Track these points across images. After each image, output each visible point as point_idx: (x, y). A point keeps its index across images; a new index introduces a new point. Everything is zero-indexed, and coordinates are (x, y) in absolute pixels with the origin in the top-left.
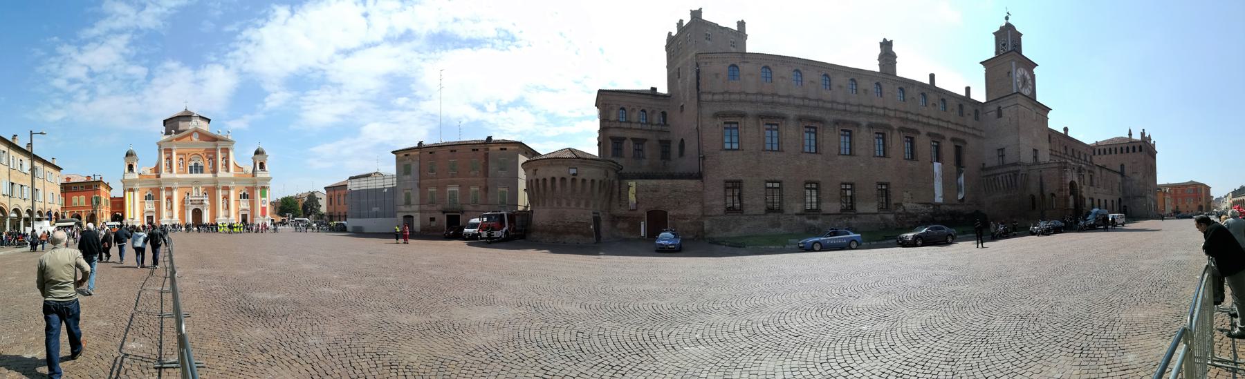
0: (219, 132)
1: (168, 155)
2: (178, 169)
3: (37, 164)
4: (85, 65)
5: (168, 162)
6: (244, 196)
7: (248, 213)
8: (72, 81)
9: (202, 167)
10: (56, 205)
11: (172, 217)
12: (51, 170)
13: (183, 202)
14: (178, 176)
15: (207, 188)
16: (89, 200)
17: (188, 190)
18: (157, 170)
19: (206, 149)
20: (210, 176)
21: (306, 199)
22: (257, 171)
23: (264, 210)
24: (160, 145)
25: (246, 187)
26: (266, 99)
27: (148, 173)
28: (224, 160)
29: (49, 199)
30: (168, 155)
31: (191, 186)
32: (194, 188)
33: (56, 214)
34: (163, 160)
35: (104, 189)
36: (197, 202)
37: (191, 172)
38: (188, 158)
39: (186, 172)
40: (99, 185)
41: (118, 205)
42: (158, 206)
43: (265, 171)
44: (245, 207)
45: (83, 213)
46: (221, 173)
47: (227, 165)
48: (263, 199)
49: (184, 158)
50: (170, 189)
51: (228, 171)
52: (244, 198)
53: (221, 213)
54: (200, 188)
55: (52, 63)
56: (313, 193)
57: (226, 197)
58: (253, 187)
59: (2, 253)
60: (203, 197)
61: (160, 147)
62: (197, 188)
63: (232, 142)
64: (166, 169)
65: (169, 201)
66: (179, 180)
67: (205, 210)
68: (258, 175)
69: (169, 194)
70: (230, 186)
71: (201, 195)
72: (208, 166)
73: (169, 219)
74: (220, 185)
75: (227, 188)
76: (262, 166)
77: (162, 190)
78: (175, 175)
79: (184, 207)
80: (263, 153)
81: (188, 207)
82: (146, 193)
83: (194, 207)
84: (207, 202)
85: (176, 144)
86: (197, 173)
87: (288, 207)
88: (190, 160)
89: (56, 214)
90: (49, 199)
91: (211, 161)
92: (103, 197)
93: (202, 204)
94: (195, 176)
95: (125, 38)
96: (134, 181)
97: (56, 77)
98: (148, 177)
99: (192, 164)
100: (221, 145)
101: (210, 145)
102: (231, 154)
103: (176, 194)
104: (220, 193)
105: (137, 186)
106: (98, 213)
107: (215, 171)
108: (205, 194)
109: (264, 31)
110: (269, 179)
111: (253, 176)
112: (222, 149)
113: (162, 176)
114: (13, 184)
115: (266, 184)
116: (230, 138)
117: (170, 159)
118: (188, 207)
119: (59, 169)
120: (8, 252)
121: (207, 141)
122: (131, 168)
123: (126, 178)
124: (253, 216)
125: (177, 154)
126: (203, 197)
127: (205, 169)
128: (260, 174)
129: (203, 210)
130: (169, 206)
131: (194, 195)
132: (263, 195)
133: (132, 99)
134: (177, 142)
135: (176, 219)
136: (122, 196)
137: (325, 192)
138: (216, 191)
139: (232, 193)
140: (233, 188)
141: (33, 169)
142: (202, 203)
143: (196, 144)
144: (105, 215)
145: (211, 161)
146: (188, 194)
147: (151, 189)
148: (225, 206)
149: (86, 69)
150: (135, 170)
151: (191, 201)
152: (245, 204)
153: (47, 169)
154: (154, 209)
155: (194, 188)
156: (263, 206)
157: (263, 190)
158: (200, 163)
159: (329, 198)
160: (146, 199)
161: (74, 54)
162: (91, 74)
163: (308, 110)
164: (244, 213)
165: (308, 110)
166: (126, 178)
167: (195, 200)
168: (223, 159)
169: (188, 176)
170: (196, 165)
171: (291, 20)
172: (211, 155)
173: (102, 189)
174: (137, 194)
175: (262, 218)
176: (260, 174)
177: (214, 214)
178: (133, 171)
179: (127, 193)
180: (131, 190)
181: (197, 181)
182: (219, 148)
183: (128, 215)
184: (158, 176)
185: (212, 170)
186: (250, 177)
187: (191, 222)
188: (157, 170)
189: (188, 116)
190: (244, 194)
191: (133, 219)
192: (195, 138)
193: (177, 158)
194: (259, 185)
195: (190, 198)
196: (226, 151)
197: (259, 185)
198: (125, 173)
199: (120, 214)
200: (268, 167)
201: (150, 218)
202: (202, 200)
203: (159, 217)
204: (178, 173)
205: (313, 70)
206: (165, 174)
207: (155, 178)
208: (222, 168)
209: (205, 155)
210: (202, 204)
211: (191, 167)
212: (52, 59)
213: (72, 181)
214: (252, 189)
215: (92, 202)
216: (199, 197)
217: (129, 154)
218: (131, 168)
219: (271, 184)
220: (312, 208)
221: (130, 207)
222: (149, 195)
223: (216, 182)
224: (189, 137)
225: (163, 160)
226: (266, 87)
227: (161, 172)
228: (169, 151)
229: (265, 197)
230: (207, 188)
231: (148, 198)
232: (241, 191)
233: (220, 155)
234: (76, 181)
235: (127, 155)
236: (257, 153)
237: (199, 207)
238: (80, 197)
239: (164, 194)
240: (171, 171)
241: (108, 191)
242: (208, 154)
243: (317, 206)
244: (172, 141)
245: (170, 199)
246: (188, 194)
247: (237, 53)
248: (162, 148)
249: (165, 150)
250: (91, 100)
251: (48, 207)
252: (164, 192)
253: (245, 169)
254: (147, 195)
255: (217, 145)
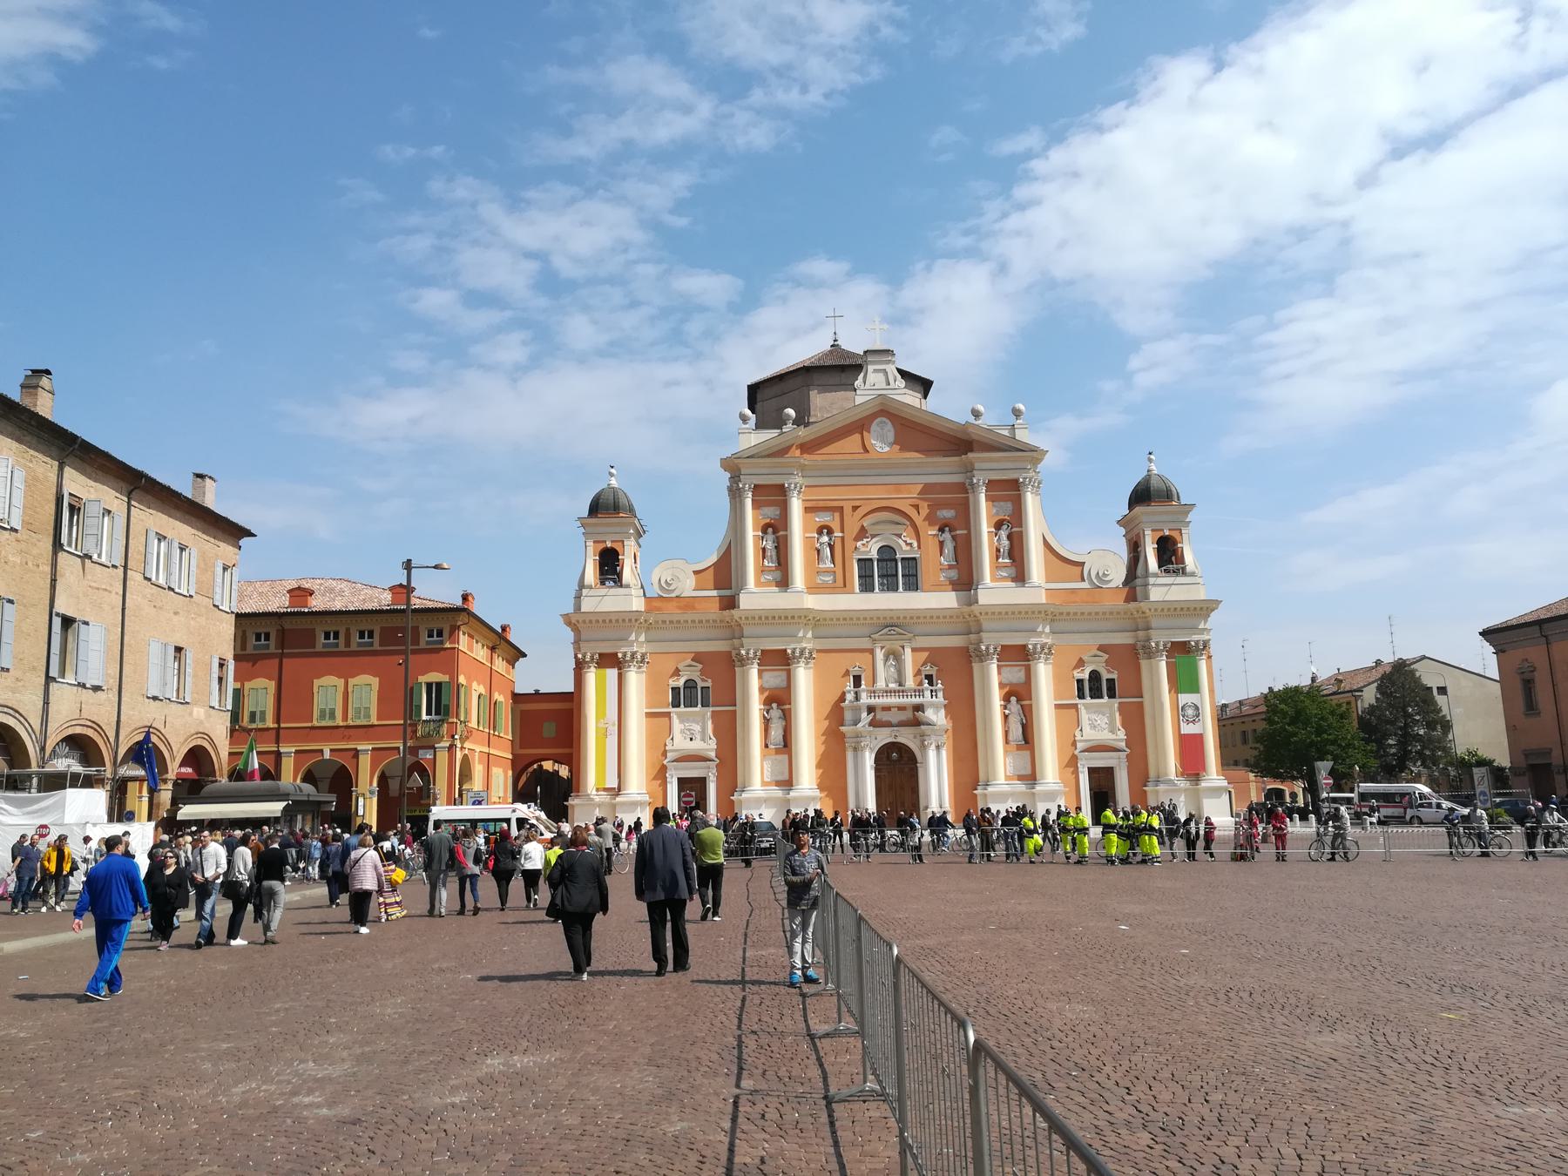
0: (976, 414)
1: (771, 512)
2: (812, 571)
3: (77, 483)
4: (530, 255)
5: (769, 545)
6: (1094, 687)
7: (1120, 766)
8: (477, 299)
9: (911, 562)
10: (199, 712)
11: (788, 783)
12: (180, 530)
13: (835, 718)
14: (812, 602)
15: (935, 656)
16: (401, 699)
17: (858, 663)
18: (725, 574)
19: (927, 489)
20: (948, 600)
21: (1370, 696)
22: (1147, 574)
23: (1191, 748)
24: (733, 467)
25: (1102, 648)
26: (1135, 362)
27: (687, 586)
28: (1003, 533)
29: (154, 671)
30: (771, 512)
31: (865, 643)
32: (880, 655)
33: (197, 757)
34: (751, 533)
35: (481, 653)
36: (894, 717)
37: (867, 587)
38: (852, 527)
39: (845, 587)
40: (454, 629)
41: (549, 730)
42: (729, 733)
43: (1184, 572)
44: (1104, 736)
45: (365, 762)
46: (994, 591)
47: (1016, 555)
48: (1184, 698)
49: (835, 525)
50: (780, 660)
51: (1020, 577)
52: (1096, 693)
53: (1001, 764)
54: (908, 656)
55: (410, 232)
56: (1401, 667)
57: (1019, 695)
58: (1133, 647)
59: (11, 947)
60: (920, 692)
61: (735, 477)
62: (894, 656)
63: (1032, 454)
64: (762, 570)
65: (776, 713)
66: (815, 621)
67: (932, 754)
68: (1156, 594)
69: (775, 679)
70: (1032, 642)
71: (910, 683)
72: (936, 560)
73: (777, 793)
74: (990, 641)
75: (1020, 655)
76: (1169, 552)
77: (744, 662)
78: (802, 597)
79: (843, 735)
80: (1167, 495)
81: (858, 736)
82: (677, 673)
83: (884, 737)
84: (937, 716)
85: (802, 468)
86: (892, 587)
87: (1303, 734)
88: (862, 533)
89: (197, 757)
90: (154, 671)
91: (947, 536)
92: (474, 690)
93: (917, 723)
94: (880, 601)
95: (680, 181)
96: (625, 621)
97: (429, 282)
98: (687, 604)
99: (872, 549)
100: (986, 468)
101: (943, 470)
102: (1031, 501)
103: (804, 679)
104: (993, 678)
105: (638, 643)
106: (442, 758)
107: (965, 581)
108: (929, 678)
109: (1120, 139)
110: (1204, 609)
111: (1132, 597)
112: (991, 485)
113: (746, 602)
114: (67, 622)
115: (1195, 629)
116: (1023, 436)
117: (777, 529)
118: (858, 736)
119: (234, 532)
120: (308, 892)
121: (926, 451)
122: (609, 564)
123: (587, 606)
124: (1141, 777)
125: (807, 510)
126: (920, 692)
127: (926, 572)
128: (1162, 590)
129: (924, 747)
130: (776, 733)
131: (881, 684)
132: (1184, 680)
133: (680, 371)
134: (807, 459)
135: (808, 793)
136: (571, 689)
137: (1485, 660)
138: (976, 666)
139: (1044, 674)
140: (1048, 650)
141: (67, 510)
142: (915, 718)
143: (884, 467)
144: (478, 770)
145: (947, 536)
146: (857, 680)
147: (698, 658)
148: (1016, 732)
149: (532, 266)
150: (627, 575)
151: (871, 709)
152: (1103, 721)
153: (148, 519)
154: (709, 747)
155: (880, 655)
156: (1187, 729)
157: (1180, 659)
158: (905, 546)
159: (1519, 685)
160: (676, 704)
161: (492, 211)
162: (550, 283)
163: (1288, 376)
164: (1101, 761)
165: (1288, 376)
166: (587, 606)
167: (887, 708)
168: (998, 525)
169: (855, 601)
170: (887, 554)
171: (1211, 90)
172: (947, 514)
173: (470, 648)
174: (635, 680)
175: (1183, 784)
176: (1162, 590)
177: (969, 773)
178: (618, 581)
179: (591, 676)
180: (609, 660)
181: (892, 626)
182: (980, 478)
183: (595, 772)
184: (730, 603)
185: (954, 574)
186: (1118, 602)
187: (871, 805)
188: (725, 574)
189: (842, 368)
190: (1095, 676)
191: (617, 791)
192: (880, 443)
193: (805, 530)
194: (1160, 638)
195: (865, 699)
196: (1010, 492)
197: (1160, 638)
198: (582, 585)
199: (564, 772)
200: (1195, 553)
201: (693, 789)
202: (919, 708)
203: (731, 780)
204: (813, 589)
205: (1301, 234)
206: (756, 595)
207: (713, 611)
208: (997, 567)
209: (925, 511)
210: (917, 723)
211: (865, 563)
212: (414, 219)
213: (317, 603)
214: (1131, 657)
215: (411, 710)
216: (901, 692)
217: (604, 507)
218: (609, 564)
219: (1216, 630)
220: (1406, 738)
221: (603, 734)
222: (690, 685)
223: (971, 624)
224: (857, 437)
225: (751, 533)
226: (1131, 322)
227: (742, 584)
228: (774, 496)
229: (1194, 688)
230: (935, 656)
231: (686, 696)
232: (1081, 663)
233: (985, 512)
234: (338, 605)
235: (596, 508)
236: (1143, 495)
237: (906, 737)
238: (352, 681)
239: (754, 681)
240: (784, 582)
241: (500, 665)
242: (935, 506)
243: (1431, 726)
244: (782, 452)
245: (779, 700)
246: (857, 680)
247: (1033, 216)
248: (746, 484)
249: (757, 489)
250: (534, 363)
251: (138, 716)
252: (754, 672)
253: (1093, 566)
254: (681, 683)
255: (969, 470)
